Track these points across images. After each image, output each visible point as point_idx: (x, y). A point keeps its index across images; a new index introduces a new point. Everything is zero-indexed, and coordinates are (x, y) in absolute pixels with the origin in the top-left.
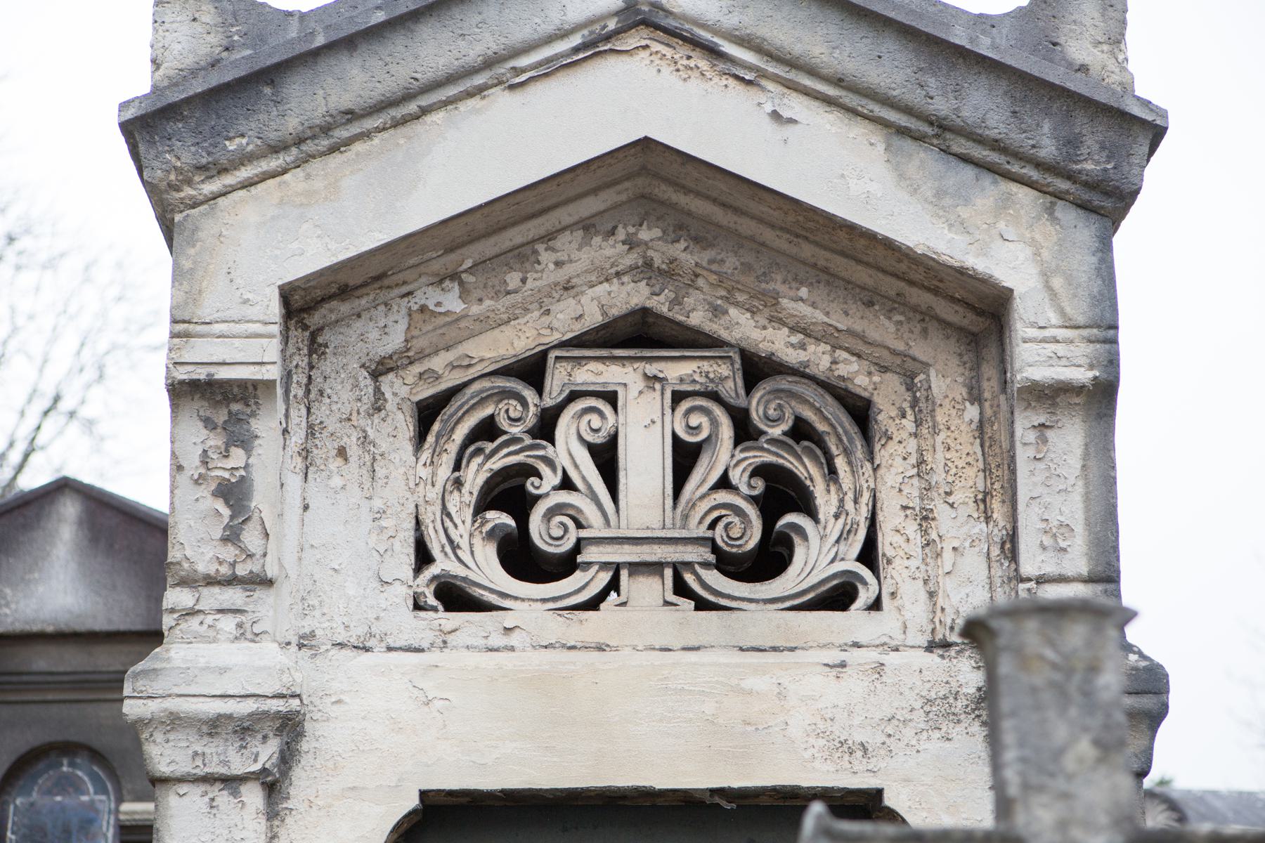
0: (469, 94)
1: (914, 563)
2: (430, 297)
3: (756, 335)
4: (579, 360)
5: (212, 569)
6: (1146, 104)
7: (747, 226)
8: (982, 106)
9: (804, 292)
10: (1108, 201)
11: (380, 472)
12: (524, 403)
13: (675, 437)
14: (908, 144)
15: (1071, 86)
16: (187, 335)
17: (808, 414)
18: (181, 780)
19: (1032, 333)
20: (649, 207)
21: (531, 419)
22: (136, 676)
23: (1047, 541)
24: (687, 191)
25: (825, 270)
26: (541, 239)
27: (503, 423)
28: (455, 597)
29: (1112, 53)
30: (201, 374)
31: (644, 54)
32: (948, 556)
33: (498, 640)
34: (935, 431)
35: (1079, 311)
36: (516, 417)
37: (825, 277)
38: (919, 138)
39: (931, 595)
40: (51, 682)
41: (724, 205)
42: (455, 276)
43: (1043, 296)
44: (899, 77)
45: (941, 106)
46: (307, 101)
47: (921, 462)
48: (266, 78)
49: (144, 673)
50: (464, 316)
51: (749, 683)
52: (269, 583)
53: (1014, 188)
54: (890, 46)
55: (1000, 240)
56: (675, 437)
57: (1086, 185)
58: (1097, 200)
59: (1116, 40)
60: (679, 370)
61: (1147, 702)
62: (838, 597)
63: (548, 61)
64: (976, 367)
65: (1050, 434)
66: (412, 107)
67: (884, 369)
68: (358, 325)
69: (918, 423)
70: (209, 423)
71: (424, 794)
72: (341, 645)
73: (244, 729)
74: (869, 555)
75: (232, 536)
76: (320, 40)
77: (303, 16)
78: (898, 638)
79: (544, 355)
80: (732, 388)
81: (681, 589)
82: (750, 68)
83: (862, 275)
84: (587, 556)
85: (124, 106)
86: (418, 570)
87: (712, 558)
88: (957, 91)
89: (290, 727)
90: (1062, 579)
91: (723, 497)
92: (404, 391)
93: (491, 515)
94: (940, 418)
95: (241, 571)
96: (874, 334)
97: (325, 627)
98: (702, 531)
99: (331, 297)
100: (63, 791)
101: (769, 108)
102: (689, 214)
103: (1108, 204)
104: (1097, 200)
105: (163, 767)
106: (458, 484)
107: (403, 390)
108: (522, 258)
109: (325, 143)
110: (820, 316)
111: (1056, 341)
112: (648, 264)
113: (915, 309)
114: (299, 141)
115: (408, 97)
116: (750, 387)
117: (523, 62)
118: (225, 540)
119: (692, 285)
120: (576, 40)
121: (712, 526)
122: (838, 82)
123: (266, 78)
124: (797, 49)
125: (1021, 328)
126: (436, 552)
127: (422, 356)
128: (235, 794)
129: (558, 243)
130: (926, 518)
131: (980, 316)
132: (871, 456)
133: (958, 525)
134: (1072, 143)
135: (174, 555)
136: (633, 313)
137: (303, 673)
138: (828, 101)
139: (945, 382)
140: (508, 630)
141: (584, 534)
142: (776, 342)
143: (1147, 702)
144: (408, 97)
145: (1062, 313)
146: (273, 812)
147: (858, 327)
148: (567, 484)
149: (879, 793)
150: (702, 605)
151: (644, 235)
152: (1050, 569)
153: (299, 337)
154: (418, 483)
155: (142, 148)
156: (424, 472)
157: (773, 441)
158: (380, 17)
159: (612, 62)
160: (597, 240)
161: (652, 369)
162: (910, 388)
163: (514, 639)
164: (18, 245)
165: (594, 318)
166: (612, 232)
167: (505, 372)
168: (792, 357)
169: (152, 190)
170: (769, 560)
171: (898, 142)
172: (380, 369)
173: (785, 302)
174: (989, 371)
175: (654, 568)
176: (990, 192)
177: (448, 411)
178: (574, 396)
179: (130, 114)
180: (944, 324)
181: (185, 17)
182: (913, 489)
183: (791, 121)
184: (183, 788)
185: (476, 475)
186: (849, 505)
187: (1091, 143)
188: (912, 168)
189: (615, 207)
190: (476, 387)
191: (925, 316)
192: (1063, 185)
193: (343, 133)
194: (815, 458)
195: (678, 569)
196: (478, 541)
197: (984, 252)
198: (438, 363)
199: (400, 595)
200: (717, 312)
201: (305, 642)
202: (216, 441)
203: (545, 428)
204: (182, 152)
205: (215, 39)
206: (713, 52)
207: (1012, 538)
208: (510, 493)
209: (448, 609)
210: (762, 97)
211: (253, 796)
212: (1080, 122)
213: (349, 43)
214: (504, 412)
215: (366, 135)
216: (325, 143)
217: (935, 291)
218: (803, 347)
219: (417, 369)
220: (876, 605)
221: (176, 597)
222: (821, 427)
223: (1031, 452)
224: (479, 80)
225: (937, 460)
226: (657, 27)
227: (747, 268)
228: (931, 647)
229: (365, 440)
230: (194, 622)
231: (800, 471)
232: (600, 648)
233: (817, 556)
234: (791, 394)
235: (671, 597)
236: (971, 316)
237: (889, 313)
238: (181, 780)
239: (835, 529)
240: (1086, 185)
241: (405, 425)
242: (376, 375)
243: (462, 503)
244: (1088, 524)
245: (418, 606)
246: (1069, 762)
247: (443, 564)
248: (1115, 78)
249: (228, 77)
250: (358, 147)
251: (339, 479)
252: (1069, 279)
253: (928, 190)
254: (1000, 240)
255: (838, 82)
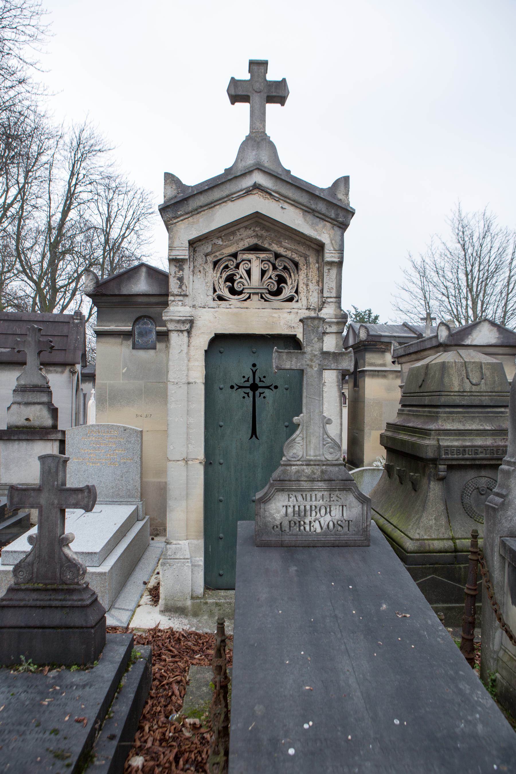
0: (223, 202)
1: (305, 293)
2: (216, 241)
3: (277, 249)
4: (244, 254)
5: (177, 293)
6: (351, 208)
7: (276, 228)
8: (321, 207)
9: (286, 241)
10: (343, 226)
11: (207, 275)
12: (233, 262)
13: (262, 269)
14: (307, 214)
15: (338, 204)
16: (172, 250)
17: (287, 265)
18: (173, 331)
19: (328, 251)
20: (257, 224)
21: (235, 265)
22: (165, 312)
23: (329, 290)
24: (265, 221)
25: (291, 237)
26: (237, 230)
27: (229, 266)
28: (221, 298)
29: (346, 197)
30: (174, 257)
31: (257, 194)
32: (311, 292)
33: (228, 306)
34: (310, 269)
35: (337, 248)
36: (232, 264)
37: (291, 238)
38: (309, 212)
39: (308, 299)
40: (141, 304)
41: (272, 224)
42: (221, 237)
43: (330, 245)
44: (306, 201)
45: (313, 207)
46: (193, 204)
47: (307, 274)
48: (185, 200)
49: (166, 312)
50: (222, 245)
51: (273, 315)
52: (187, 296)
53: (326, 223)
54: (304, 194)
55: (324, 234)
56: (262, 269)
57: (340, 223)
58: (342, 226)
59: (347, 194)
60: (263, 256)
61: (344, 320)
62: (290, 299)
63: (239, 196)
64: (318, 257)
65: (330, 271)
66: (213, 205)
67: (301, 256)
68: (202, 247)
69: (307, 267)
70: (176, 266)
71: (215, 334)
72: (200, 307)
73: (184, 322)
74: (297, 292)
75: (180, 287)
76: (195, 192)
77: (192, 187)
78: (301, 307)
79: (237, 253)
80: (272, 259)
81: (262, 297)
82: (277, 198)
83: (298, 238)
84: (245, 291)
85: (159, 206)
86: (214, 293)
87: (268, 292)
88: (317, 204)
89: (191, 322)
90: (331, 297)
91: (270, 280)
92: (211, 259)
93: (227, 283)
94: (311, 266)
95: (182, 293)
96: (299, 250)
97: (198, 303)
98: (266, 287)
99: (197, 241)
100: (145, 325)
101: (281, 206)
102: (265, 225)
103: (344, 227)
104: (342, 226)
105: (170, 329)
106: (221, 277)
107: (211, 259)
108: (233, 234)
109: (196, 212)
110: (289, 246)
111: (332, 253)
112: (257, 235)
113: (307, 245)
114: (191, 212)
115: (212, 203)
116: (276, 259)
117: (234, 196)
118: (179, 288)
119: (266, 239)
120: (244, 192)
121: (268, 286)
122: (294, 201)
123: (185, 200)
124: (287, 194)
125: (326, 251)
126: (217, 290)
127: (214, 252)
128: (182, 333)
129: (240, 231)
130: (307, 285)
131: (319, 248)
132: (298, 273)
133: (313, 287)
134: (337, 215)
135: (170, 290)
136: (254, 244)
137: (193, 312)
138: (292, 205)
139: (312, 260)
140: (230, 305)
141: (244, 287)
142: (281, 251)
143: (344, 320)
144: (212, 203)
145: (334, 248)
146: (189, 337)
147: (296, 248)
148: (241, 277)
149: (296, 335)
150: (266, 301)
151: (257, 229)
152: (329, 296)
153: (192, 249)
154: (213, 276)
155: (163, 214)
156: (215, 275)
157: (280, 270)
158: (207, 187)
159: (251, 196)
160: (248, 230)
161: (257, 255)
162: (306, 260)
163: (231, 306)
164: (119, 189)
165: (247, 245)
166: (250, 229)
167: (230, 256)
168: (284, 254)
169: (164, 221)
170: (278, 292)
171: (305, 213)
172: (207, 255)
173: (283, 243)
174: (320, 257)
175: (257, 294)
176: (321, 224)
177: (219, 263)
178: (243, 261)
179: (160, 207)
180: (313, 248)
181: (170, 187)
182: (305, 280)
183: (285, 209)
184: (173, 332)
185: (224, 276)
186: (293, 282)
187: (341, 215)
188: (307, 219)
189: (251, 223)
190: (224, 258)
191: (309, 247)
192: (335, 223)
193: (200, 210)
194: (287, 273)
195: (261, 294)
196: (225, 288)
197: (320, 236)
198: (217, 254)
199: (211, 298)
200: (270, 244)
201: (194, 306)
202: (177, 269)
203: (237, 267)
204: (170, 215)
205: (175, 192)
206: (270, 194)
207: (323, 289)
208: (230, 279)
209: (219, 300)
210: (279, 204)
211: (186, 334)
212: (339, 211)
213: (201, 193)
214: (230, 263)
215: (204, 211)
216: (196, 212)
217: (311, 242)
218: (286, 252)
219: (213, 255)
220: (297, 301)
221: (171, 298)
222: (289, 267)
223: (327, 274)
224: (225, 200)
225: (310, 274)
226: (260, 189)
227: (276, 236)
228: (307, 309)
229: (204, 269)
230: (174, 303)
231: (285, 276)
232: (247, 308)
233: (287, 292)
234: (283, 261)
235: (260, 299)
236: (318, 247)
237: (302, 246)
238: (173, 331)
239: (291, 287)
240: (340, 223)
241: (211, 266)
242: (206, 256)
243: (222, 281)
244: (336, 287)
245: (214, 300)
246: (313, 341)
247: (218, 292)
248: (346, 202)
249: (178, 200)
250: (203, 213)
251: (199, 276)
252: (336, 241)
253: (310, 223)
254: (324, 234)
255: (294, 201)
